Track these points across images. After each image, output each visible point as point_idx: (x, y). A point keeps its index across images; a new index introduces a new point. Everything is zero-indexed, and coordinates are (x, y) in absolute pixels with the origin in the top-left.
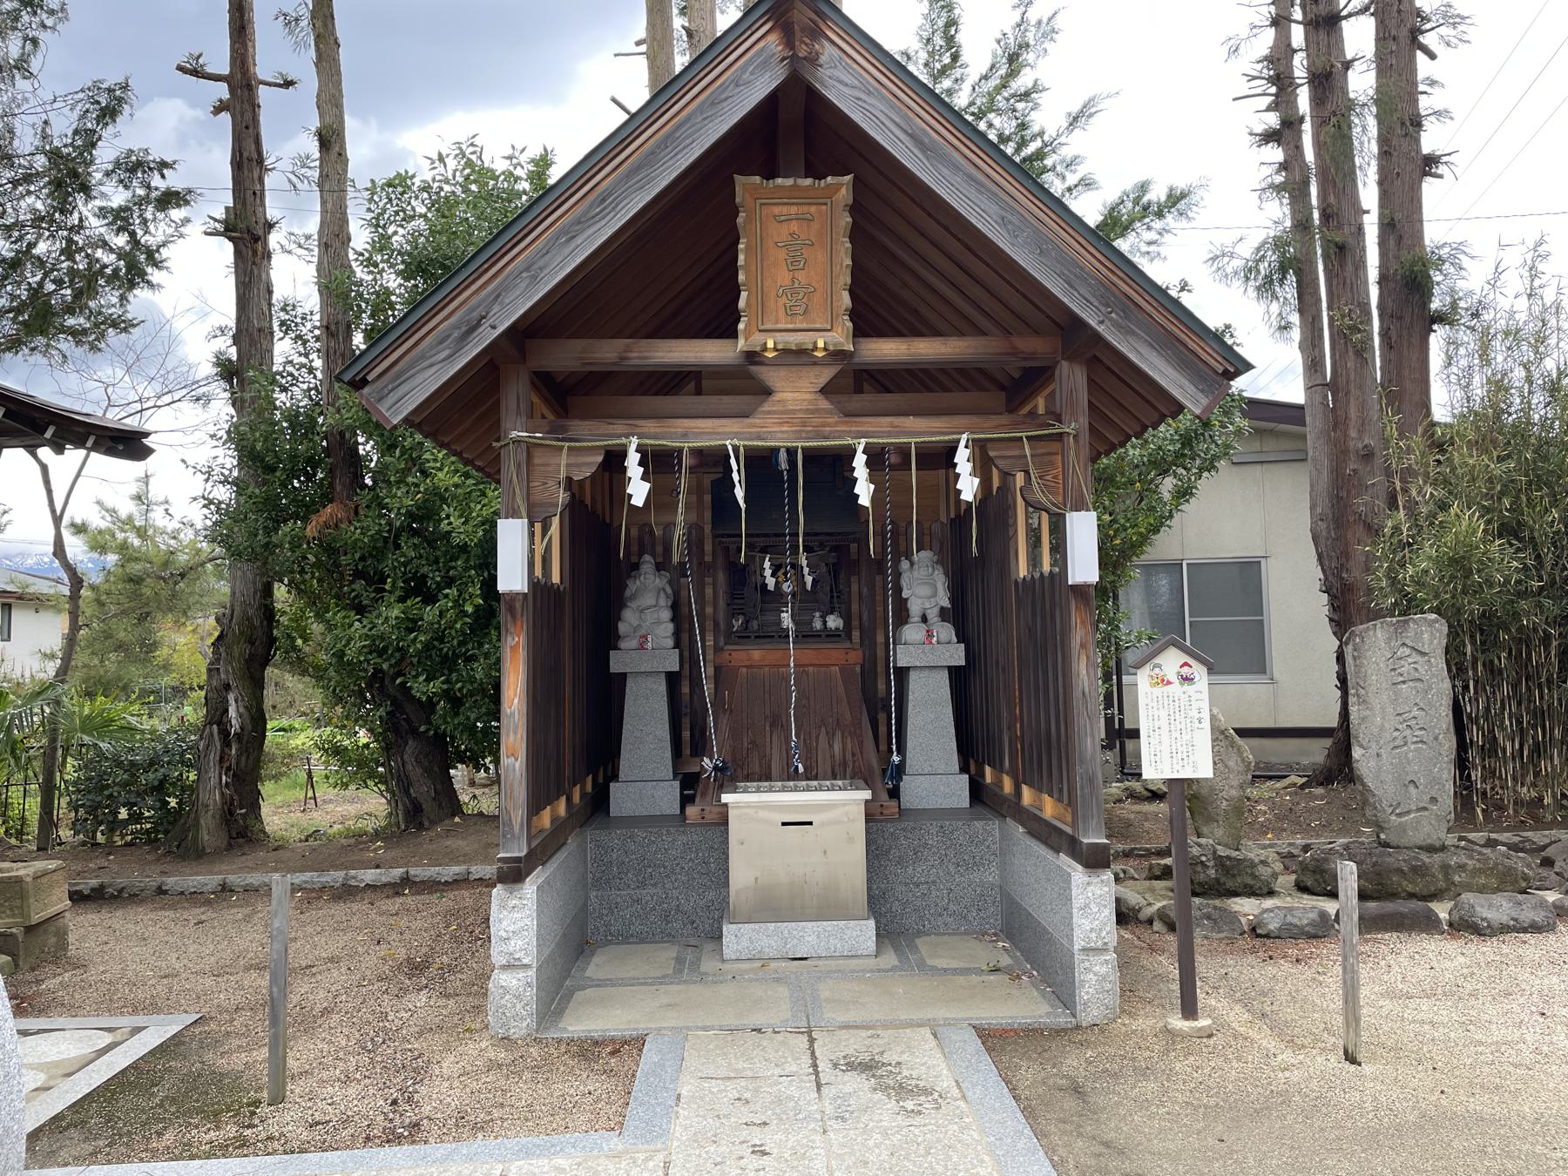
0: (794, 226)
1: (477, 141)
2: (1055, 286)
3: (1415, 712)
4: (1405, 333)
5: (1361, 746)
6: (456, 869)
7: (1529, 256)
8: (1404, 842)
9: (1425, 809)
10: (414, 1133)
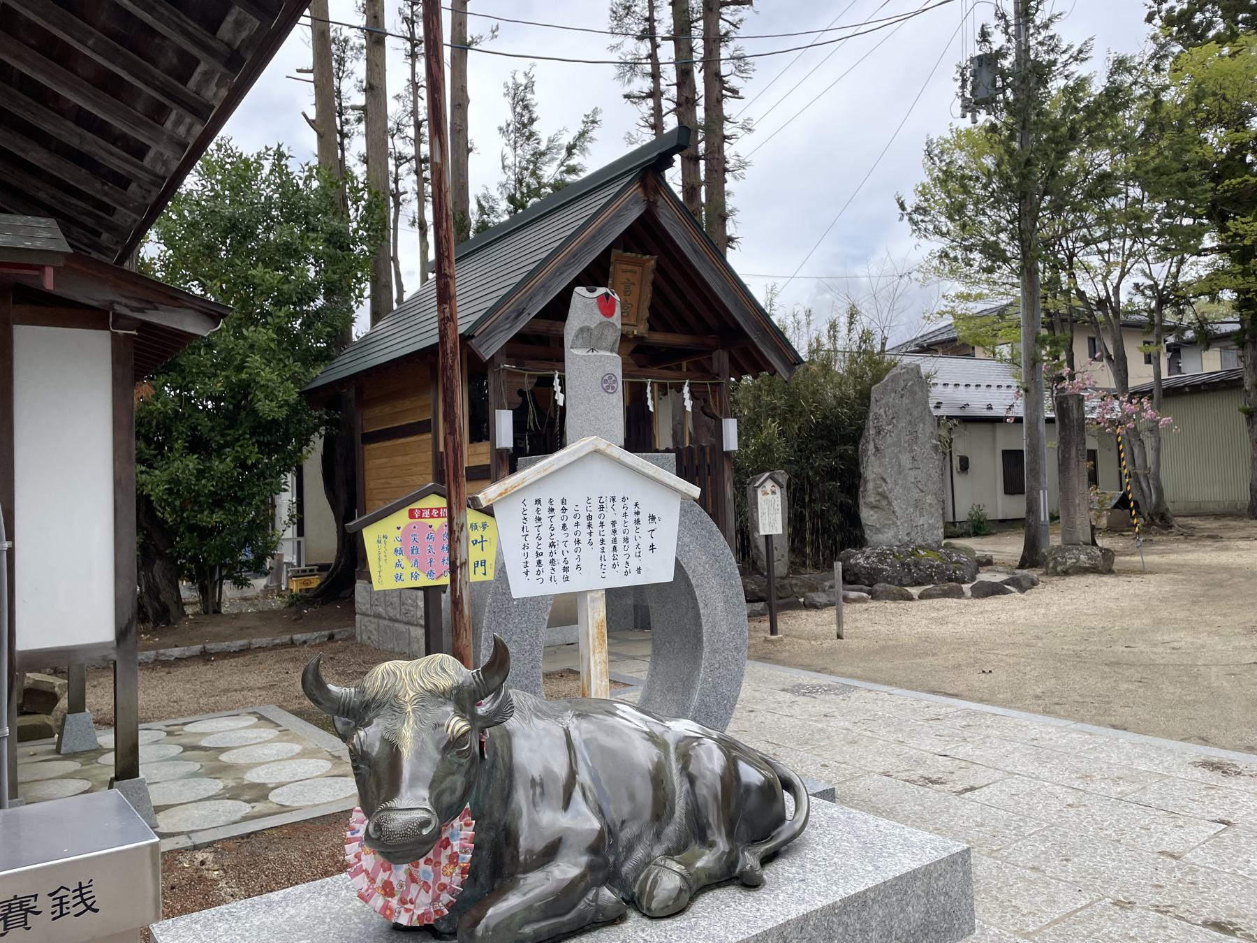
0: (628, 275)
1: (911, 201)
2: (740, 320)
6: (242, 642)
10: (1110, 572)
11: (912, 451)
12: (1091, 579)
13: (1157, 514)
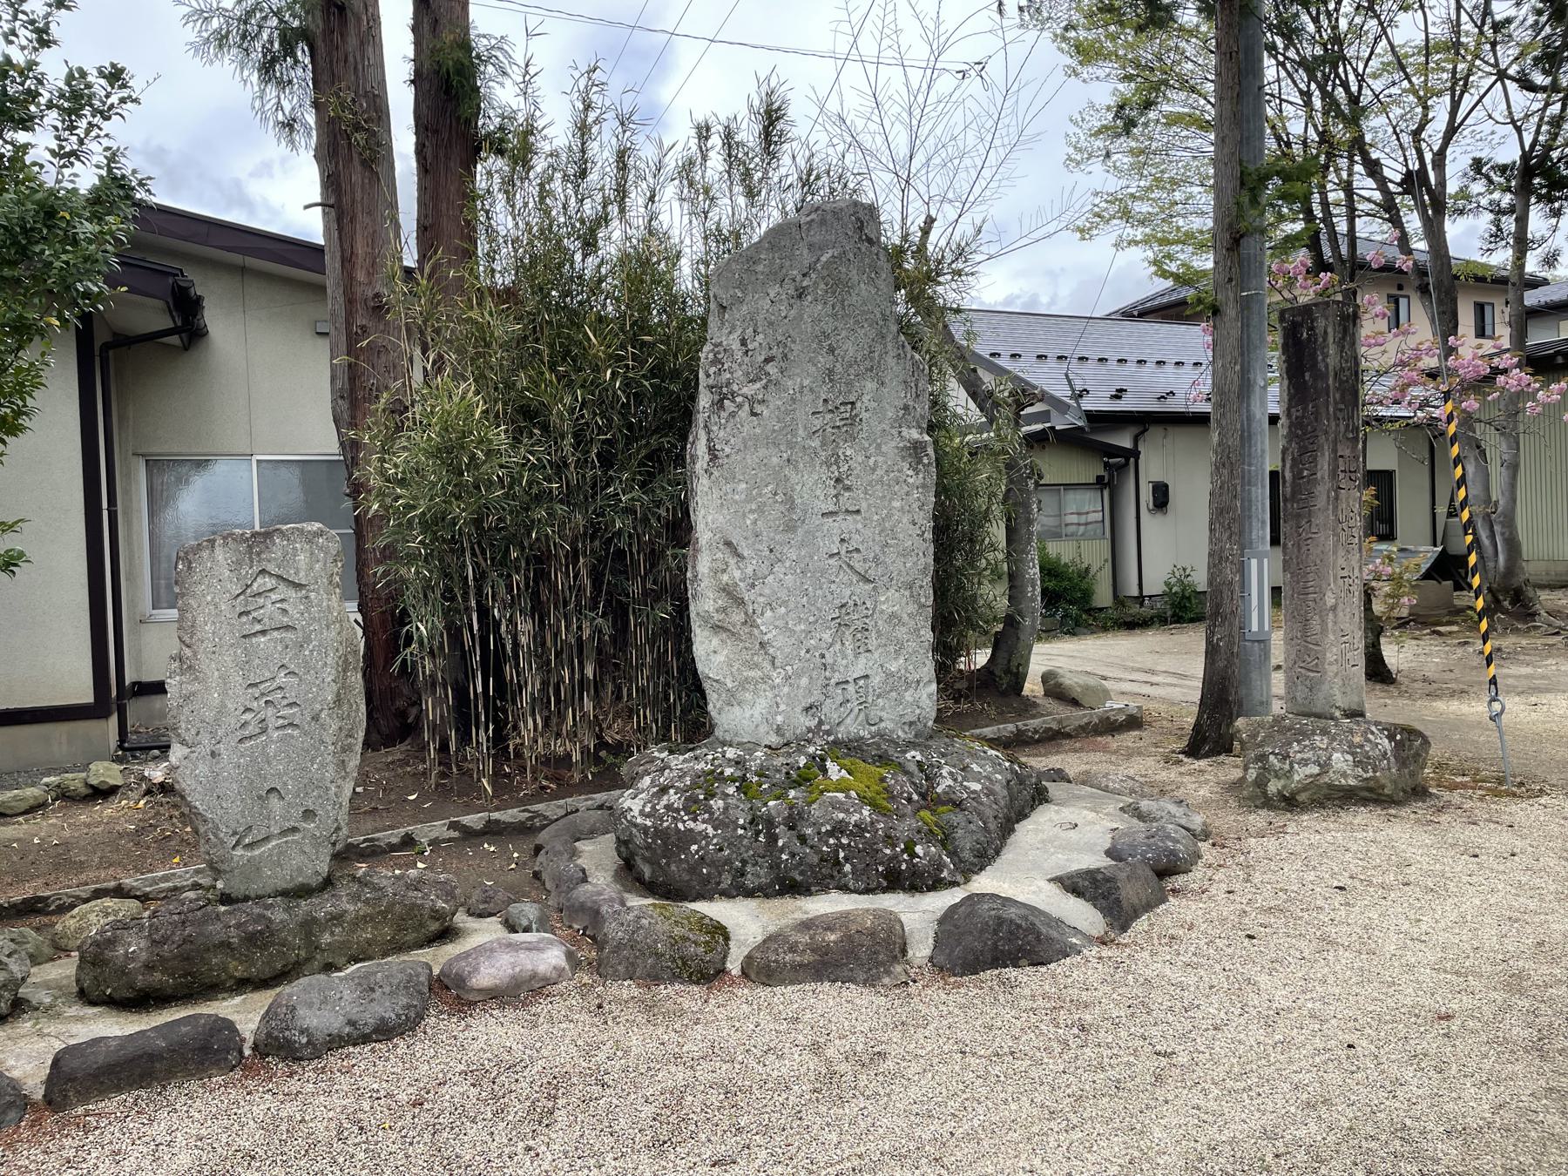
3: (282, 679)
4: (441, 154)
5: (183, 742)
7: (582, 83)
8: (255, 888)
9: (294, 830)
10: (1419, 792)
11: (834, 460)
12: (1362, 816)
13: (1506, 591)
